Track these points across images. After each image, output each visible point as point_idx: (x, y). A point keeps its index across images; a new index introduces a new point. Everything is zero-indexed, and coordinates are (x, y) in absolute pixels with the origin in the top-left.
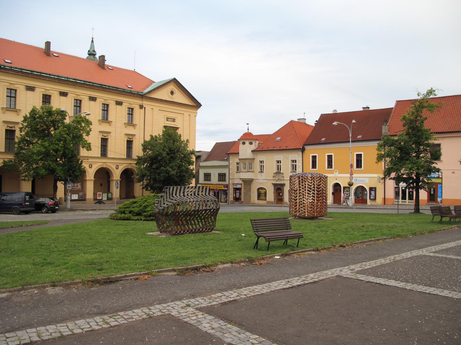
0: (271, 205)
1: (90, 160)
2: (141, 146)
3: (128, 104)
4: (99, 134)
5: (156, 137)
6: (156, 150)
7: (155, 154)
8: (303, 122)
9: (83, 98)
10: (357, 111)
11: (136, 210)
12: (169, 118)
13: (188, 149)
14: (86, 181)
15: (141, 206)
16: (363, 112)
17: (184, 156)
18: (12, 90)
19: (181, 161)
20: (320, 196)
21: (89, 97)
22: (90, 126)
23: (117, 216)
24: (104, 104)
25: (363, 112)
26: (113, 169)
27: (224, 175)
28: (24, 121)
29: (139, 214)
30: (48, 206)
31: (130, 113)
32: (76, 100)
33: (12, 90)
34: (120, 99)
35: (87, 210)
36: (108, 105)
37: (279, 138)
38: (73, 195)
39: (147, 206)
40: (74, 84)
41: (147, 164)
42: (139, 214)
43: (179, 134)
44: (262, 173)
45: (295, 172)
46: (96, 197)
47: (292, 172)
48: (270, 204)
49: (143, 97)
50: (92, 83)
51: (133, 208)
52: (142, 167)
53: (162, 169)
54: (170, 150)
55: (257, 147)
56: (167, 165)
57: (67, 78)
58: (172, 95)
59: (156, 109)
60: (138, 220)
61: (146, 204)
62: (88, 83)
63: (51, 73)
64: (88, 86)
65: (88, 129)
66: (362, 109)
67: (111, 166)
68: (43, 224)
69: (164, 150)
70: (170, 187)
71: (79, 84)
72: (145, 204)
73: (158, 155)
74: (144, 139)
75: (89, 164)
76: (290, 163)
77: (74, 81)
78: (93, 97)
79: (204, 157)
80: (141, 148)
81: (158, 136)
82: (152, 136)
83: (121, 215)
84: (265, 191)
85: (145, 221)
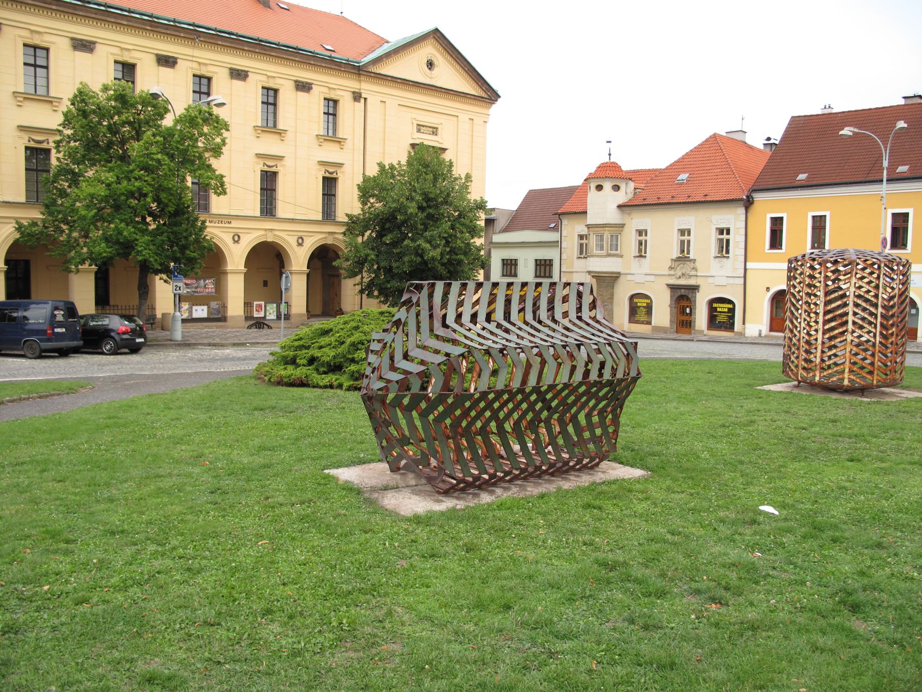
0: (664, 336)
1: (235, 224)
2: (356, 188)
3: (325, 90)
4: (256, 160)
5: (392, 167)
6: (393, 198)
7: (390, 207)
8: (739, 139)
9: (216, 73)
10: (888, 105)
11: (328, 355)
12: (424, 126)
13: (469, 196)
14: (225, 273)
15: (343, 343)
16: (905, 107)
17: (460, 215)
18: (37, 50)
19: (453, 227)
20: (891, 322)
21: (231, 69)
22: (223, 131)
23: (271, 373)
24: (268, 89)
25: (905, 107)
26: (290, 245)
27: (548, 262)
28: (64, 125)
29: (335, 368)
30: (117, 337)
31: (331, 111)
32: (198, 79)
33: (37, 50)
34: (306, 75)
35: (222, 346)
36: (276, 91)
37: (684, 176)
38: (194, 308)
39: (359, 343)
40: (192, 37)
41: (371, 234)
42: (335, 368)
43: (447, 160)
44: (642, 259)
45: (724, 257)
46: (252, 311)
47: (717, 257)
48: (659, 334)
49: (361, 72)
50: (236, 35)
51: (321, 347)
52: (360, 239)
53: (407, 246)
54: (427, 199)
55: (631, 196)
56: (419, 234)
57: (174, 21)
58: (430, 69)
59: (392, 103)
60: (331, 387)
61: (357, 337)
62: (227, 35)
63: (132, 8)
64: (226, 41)
65: (218, 140)
66: (902, 102)
67: (286, 237)
68: (59, 395)
69: (410, 199)
70: (433, 285)
71: (204, 37)
72: (352, 339)
73: (397, 210)
74: (363, 174)
75: (233, 234)
76: (714, 236)
77: (192, 28)
78: (238, 70)
79: (501, 223)
80: (356, 193)
81: (397, 166)
82: (381, 166)
83: (285, 369)
84: (649, 301)
85: (352, 392)
